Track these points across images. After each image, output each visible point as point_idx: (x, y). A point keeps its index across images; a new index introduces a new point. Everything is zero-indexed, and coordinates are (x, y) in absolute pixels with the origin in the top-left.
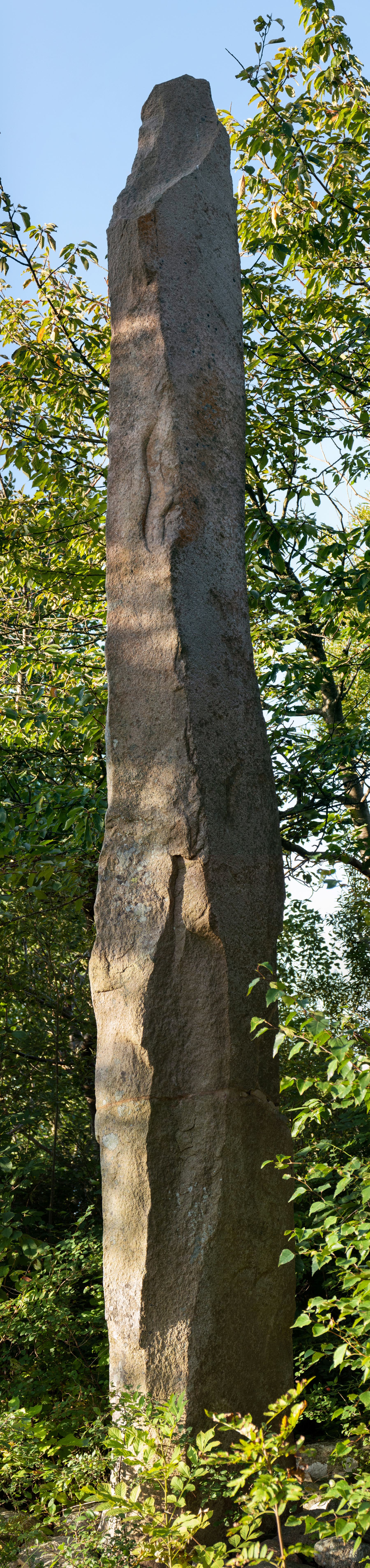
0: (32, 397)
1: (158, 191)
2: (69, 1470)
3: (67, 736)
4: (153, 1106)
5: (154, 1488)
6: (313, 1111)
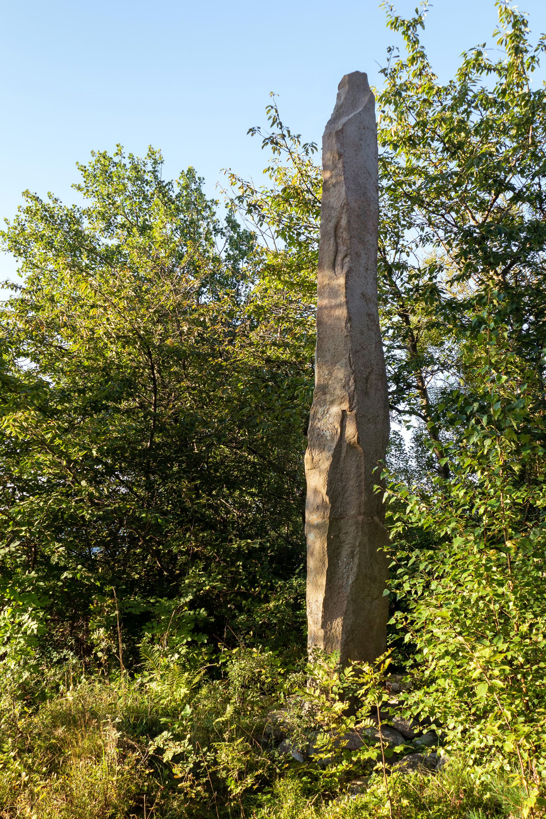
0: (289, 208)
1: (344, 120)
5: (325, 691)
6: (399, 527)
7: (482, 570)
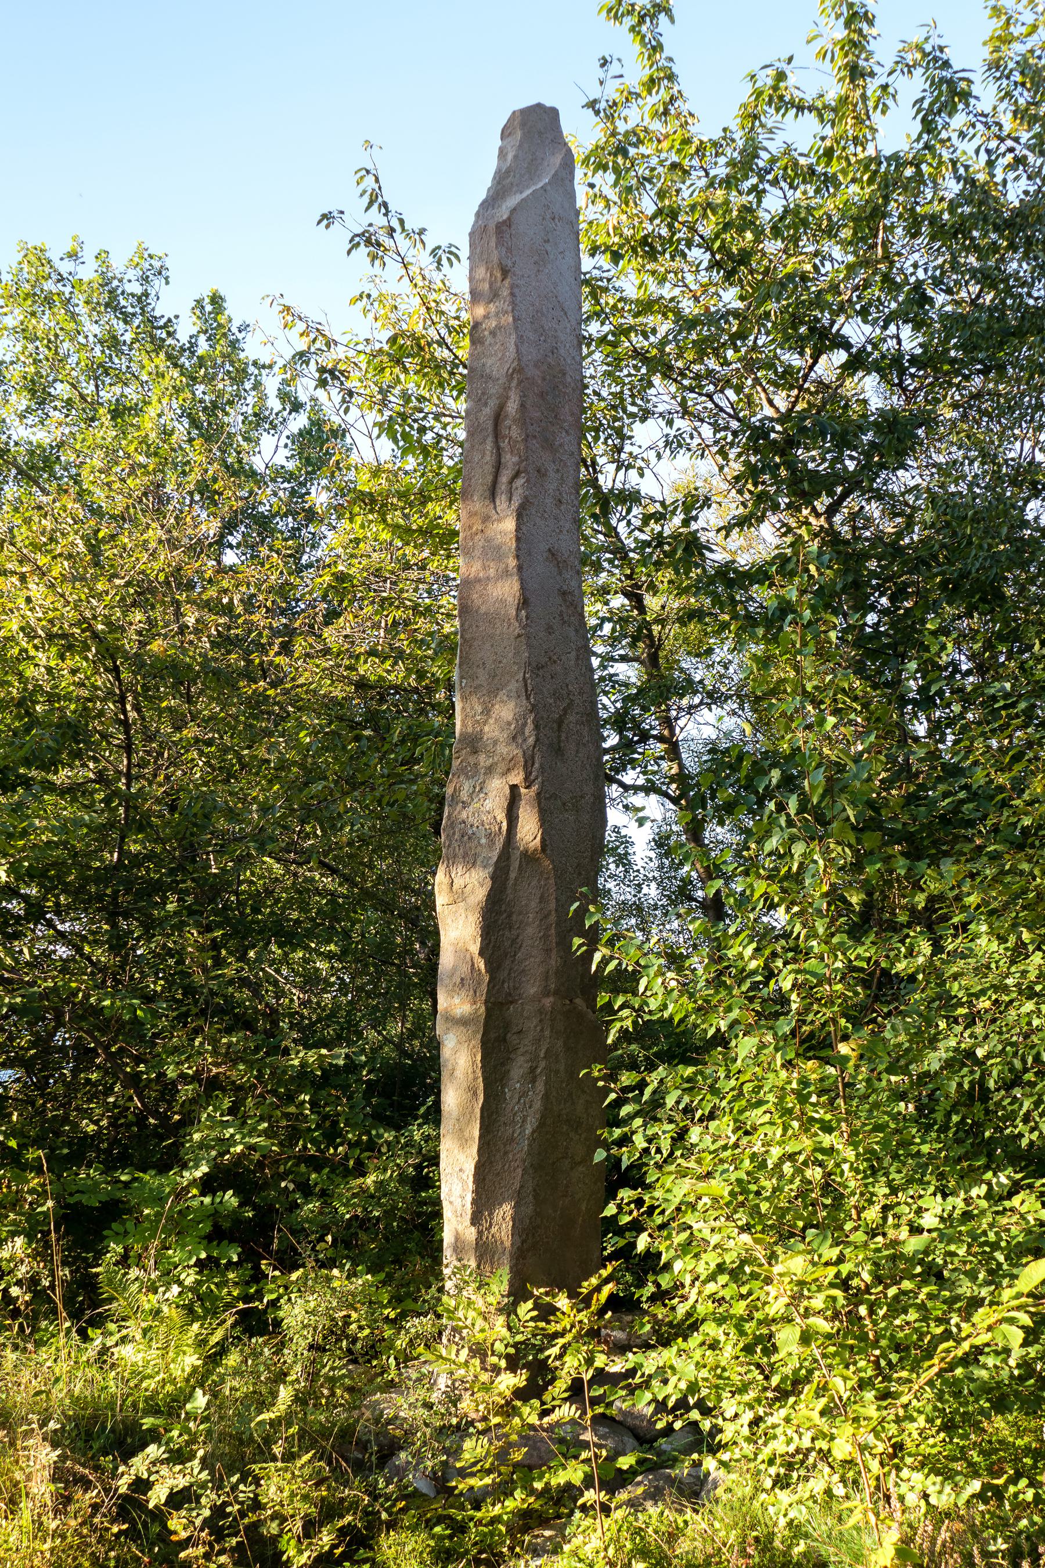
0: (402, 377)
1: (513, 201)
2: (408, 1332)
3: (421, 675)
4: (488, 1010)
5: (479, 1351)
6: (626, 1020)
7: (790, 1101)
